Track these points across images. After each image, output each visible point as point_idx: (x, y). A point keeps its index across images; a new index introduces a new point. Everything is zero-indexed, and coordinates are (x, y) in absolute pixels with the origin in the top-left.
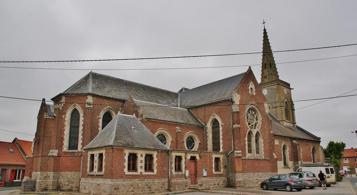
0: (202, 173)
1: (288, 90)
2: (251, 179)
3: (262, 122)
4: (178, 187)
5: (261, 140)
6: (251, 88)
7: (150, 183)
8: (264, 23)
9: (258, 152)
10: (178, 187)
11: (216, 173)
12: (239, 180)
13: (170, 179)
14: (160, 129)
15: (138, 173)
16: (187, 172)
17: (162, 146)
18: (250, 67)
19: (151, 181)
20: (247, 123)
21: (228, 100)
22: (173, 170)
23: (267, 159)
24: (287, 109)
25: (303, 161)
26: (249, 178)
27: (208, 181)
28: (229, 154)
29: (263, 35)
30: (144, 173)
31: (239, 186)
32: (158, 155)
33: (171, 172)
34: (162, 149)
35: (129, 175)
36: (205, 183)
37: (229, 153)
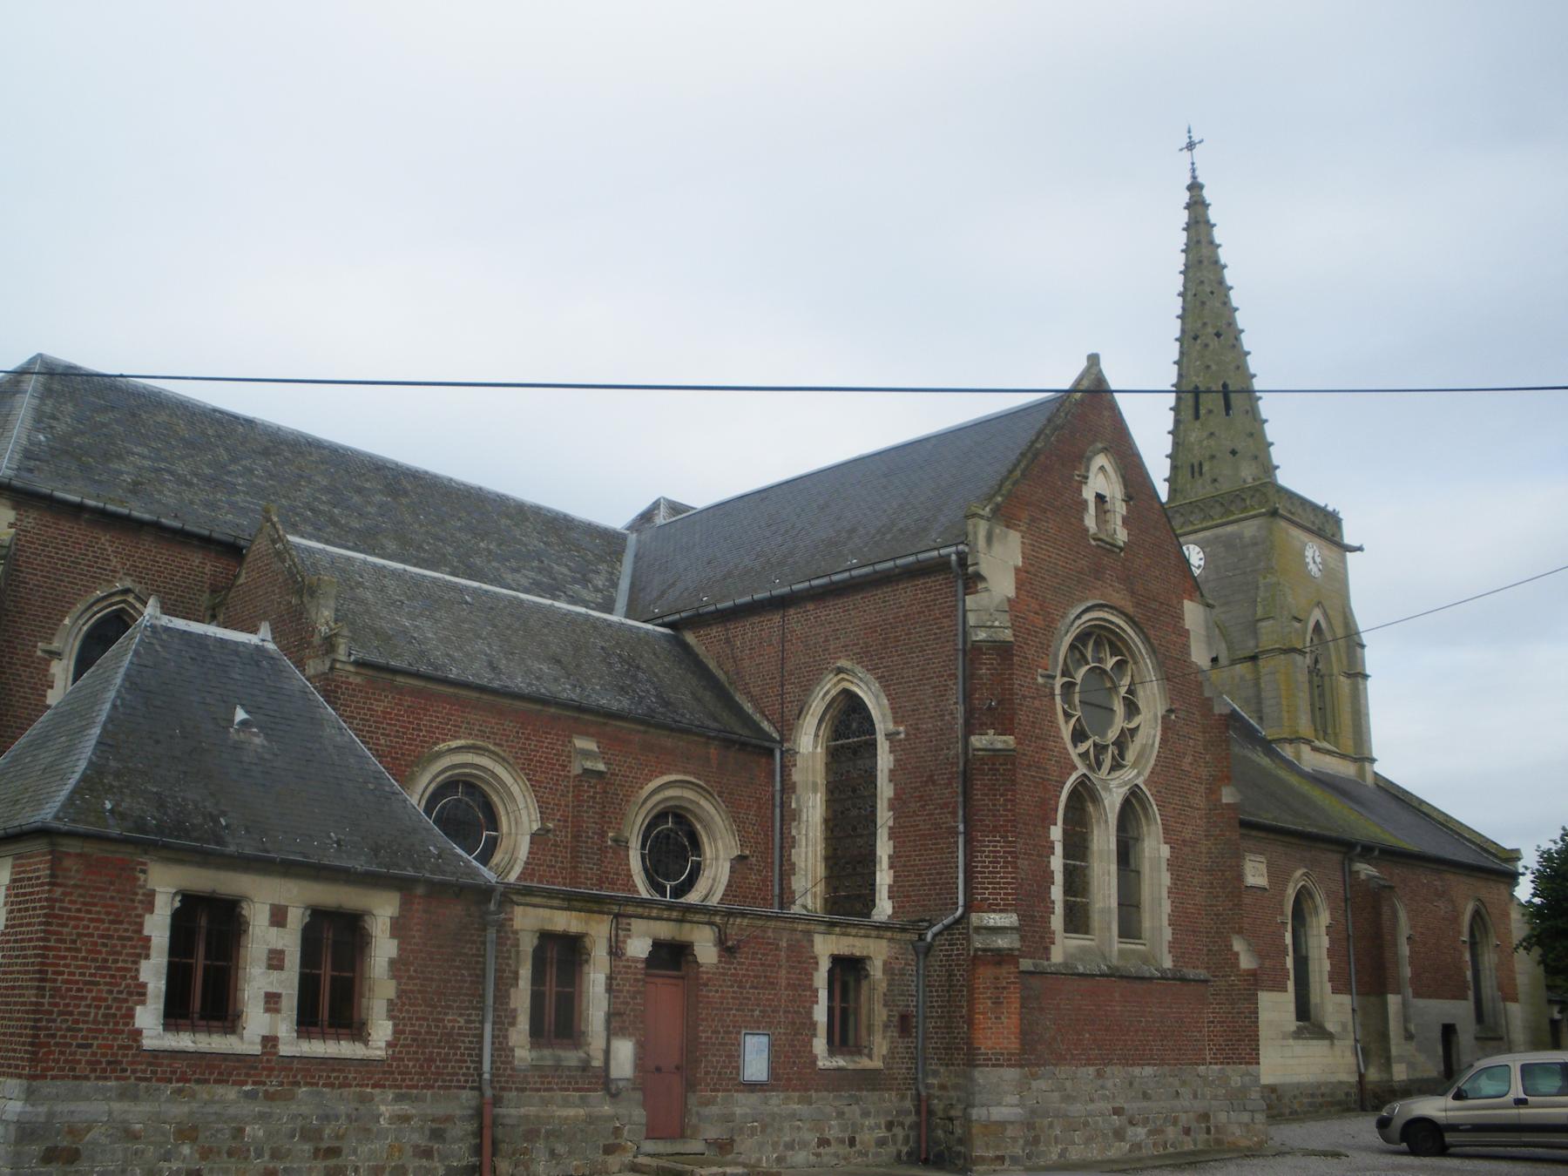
0: (734, 1058)
1: (1331, 553)
2: (1077, 1109)
3: (1165, 730)
4: (553, 1154)
5: (1155, 849)
6: (1100, 498)
7: (337, 1118)
8: (1191, 146)
9: (1129, 928)
10: (553, 1154)
11: (840, 1062)
12: (998, 1113)
13: (488, 1093)
14: (454, 744)
15: (247, 1041)
16: (624, 1053)
17: (439, 856)
18: (1094, 360)
19: (341, 1103)
20: (1066, 732)
21: (941, 566)
22: (520, 1034)
23: (1190, 973)
24: (1323, 672)
25: (1417, 995)
26: (1068, 1098)
27: (773, 1116)
28: (935, 935)
29: (1183, 217)
30: (291, 1045)
31: (991, 1154)
32: (401, 916)
33: (502, 1049)
34: (438, 877)
35: (175, 1054)
36: (753, 1131)
37: (935, 929)
